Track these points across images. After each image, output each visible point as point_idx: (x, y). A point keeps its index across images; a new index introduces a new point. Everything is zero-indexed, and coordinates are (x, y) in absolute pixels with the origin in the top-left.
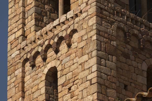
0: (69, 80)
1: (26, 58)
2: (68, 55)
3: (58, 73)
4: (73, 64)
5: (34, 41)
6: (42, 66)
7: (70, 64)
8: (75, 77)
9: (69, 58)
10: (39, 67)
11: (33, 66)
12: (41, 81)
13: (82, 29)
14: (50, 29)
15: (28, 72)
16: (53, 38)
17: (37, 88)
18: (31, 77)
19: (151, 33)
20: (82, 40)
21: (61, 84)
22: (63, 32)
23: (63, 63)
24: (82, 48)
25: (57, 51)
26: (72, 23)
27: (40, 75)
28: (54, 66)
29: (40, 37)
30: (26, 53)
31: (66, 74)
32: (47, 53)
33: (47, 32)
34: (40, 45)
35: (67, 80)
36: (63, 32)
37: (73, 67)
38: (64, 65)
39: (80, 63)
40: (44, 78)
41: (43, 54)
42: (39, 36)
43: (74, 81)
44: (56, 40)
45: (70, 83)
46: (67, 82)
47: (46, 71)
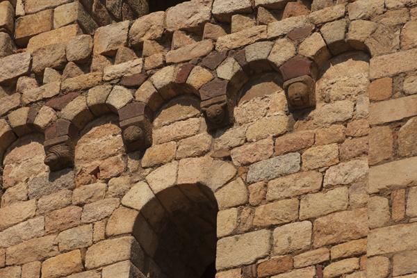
0: (292, 253)
1: (24, 122)
2: (290, 148)
3: (219, 213)
4: (320, 190)
5: (84, 64)
6: (116, 170)
7: (304, 186)
8: (333, 245)
9: (294, 158)
10: (96, 172)
11: (60, 165)
12: (107, 237)
13: (400, 48)
14: (188, 22)
15: (22, 186)
16: (210, 61)
17: (78, 261)
18: (38, 212)
19: (415, 235)
20: (394, 92)
21: (238, 263)
22: (273, 46)
23: (251, 175)
24: (396, 125)
25: (219, 123)
26: (339, 15)
27: (99, 208)
28: (195, 182)
29: (121, 48)
30: (27, 105)
31: (272, 227)
32: (152, 121)
33: (64, 63)
34: (123, 82)
35: (278, 250)
36: (276, 47)
37: (317, 203)
38: (261, 184)
39: (383, 186)
40: (125, 223)
41: (141, 118)
42: (119, 43)
43: (326, 263)
44: (227, 71)
45: (293, 268)
46: (280, 260)
47: (140, 196)
